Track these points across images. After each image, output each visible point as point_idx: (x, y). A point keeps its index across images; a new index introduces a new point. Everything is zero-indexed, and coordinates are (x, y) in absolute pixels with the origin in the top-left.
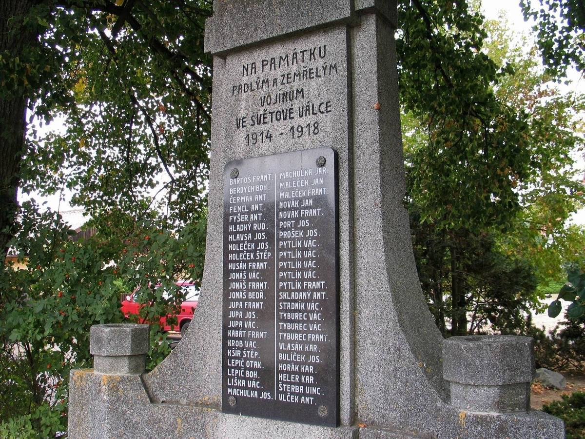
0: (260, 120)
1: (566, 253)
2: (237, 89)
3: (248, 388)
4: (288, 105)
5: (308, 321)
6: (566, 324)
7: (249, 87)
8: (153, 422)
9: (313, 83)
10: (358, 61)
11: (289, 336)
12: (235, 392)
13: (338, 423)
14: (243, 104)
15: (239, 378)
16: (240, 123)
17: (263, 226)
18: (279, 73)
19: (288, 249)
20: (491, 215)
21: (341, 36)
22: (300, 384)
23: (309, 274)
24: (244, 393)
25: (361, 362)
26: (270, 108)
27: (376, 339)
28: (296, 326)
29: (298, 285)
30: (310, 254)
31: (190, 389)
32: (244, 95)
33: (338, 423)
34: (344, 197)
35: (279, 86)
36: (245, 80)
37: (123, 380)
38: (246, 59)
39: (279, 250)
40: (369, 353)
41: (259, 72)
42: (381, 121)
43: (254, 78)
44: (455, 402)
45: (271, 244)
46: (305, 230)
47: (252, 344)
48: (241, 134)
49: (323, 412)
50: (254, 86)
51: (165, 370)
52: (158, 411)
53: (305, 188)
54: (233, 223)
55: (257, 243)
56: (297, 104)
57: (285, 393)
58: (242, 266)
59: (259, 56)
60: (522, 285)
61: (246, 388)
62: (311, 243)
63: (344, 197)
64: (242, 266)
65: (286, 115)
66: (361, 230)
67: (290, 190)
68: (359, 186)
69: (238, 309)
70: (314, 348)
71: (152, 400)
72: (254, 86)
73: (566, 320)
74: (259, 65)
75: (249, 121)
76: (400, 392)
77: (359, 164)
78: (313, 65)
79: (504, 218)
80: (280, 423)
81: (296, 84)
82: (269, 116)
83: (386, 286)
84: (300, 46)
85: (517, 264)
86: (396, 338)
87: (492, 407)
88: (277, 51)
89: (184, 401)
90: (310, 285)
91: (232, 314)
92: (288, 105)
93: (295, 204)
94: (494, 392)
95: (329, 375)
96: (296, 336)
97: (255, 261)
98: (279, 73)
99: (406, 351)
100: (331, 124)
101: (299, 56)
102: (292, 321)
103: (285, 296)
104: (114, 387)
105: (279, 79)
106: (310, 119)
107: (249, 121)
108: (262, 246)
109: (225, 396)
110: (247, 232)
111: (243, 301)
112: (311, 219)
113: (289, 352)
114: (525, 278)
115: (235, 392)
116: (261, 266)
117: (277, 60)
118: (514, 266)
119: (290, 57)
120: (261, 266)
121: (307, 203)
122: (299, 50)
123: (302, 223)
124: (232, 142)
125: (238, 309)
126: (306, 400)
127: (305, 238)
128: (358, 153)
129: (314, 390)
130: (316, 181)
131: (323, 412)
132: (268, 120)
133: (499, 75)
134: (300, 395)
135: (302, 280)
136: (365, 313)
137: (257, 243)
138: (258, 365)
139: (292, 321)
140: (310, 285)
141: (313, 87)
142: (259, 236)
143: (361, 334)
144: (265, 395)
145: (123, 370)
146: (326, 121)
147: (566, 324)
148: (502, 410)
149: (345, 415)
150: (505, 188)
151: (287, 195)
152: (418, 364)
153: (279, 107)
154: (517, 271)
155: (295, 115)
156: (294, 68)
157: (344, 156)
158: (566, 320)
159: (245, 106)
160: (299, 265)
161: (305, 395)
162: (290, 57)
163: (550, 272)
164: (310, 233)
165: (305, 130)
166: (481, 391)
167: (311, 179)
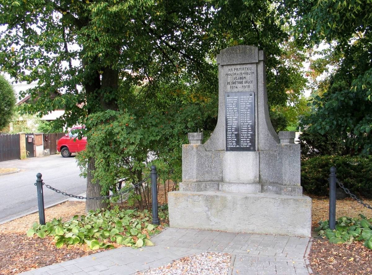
0: (234, 83)
1: (299, 111)
2: (227, 75)
3: (234, 145)
4: (242, 80)
5: (248, 129)
6: (299, 141)
7: (231, 75)
8: (206, 156)
9: (248, 76)
10: (259, 72)
11: (243, 133)
12: (230, 146)
13: (255, 151)
14: (229, 79)
15: (230, 143)
16: (228, 83)
17: (236, 109)
18: (239, 72)
19: (243, 114)
20: (279, 101)
21: (255, 66)
22: (246, 143)
23: (248, 119)
24: (232, 146)
25: (259, 138)
26: (237, 81)
27: (263, 133)
28: (245, 131)
29: (246, 122)
30: (248, 115)
31: (215, 147)
32: (229, 77)
33: (255, 151)
34: (256, 103)
35: (233, 71)
36: (229, 73)
37: (199, 146)
38: (230, 67)
39: (241, 114)
40: (261, 136)
41: (233, 71)
42: (264, 86)
43: (232, 72)
44: (281, 143)
45: (239, 112)
46: (247, 110)
47: (234, 135)
48: (229, 86)
49: (252, 148)
50: (232, 75)
51: (208, 143)
52: (208, 153)
53: (247, 100)
54: (228, 107)
55: (235, 112)
56: (244, 81)
57: (243, 145)
58: (231, 117)
59: (233, 67)
60: (281, 125)
61: (232, 145)
62: (248, 113)
63: (256, 103)
64: (231, 117)
65: (241, 83)
66: (259, 110)
67: (243, 101)
68: (259, 100)
69: (230, 127)
70: (249, 135)
71: (206, 151)
72: (232, 75)
73: (299, 140)
74: (233, 69)
75: (231, 83)
76: (268, 143)
77: (259, 95)
78: (248, 71)
79: (283, 102)
80: (241, 152)
81: (244, 76)
82: (236, 83)
83: (265, 122)
84: (244, 66)
85: (279, 116)
86: (267, 132)
87: (288, 143)
88: (238, 67)
89: (213, 150)
90: (249, 122)
91: (228, 129)
92: (242, 80)
93: (245, 104)
94: (289, 140)
95: (253, 141)
96: (245, 133)
97: (234, 116)
98: (239, 72)
99: (270, 135)
100: (252, 86)
101: (244, 69)
102: (244, 129)
103: (242, 124)
104: (197, 148)
105: (239, 74)
106: (247, 84)
107: (231, 83)
108: (236, 113)
109: (227, 147)
110: (232, 110)
111: (231, 125)
112: (248, 107)
113: (243, 136)
114: (283, 122)
115: (230, 146)
116: (236, 117)
117: (238, 69)
118: (278, 117)
119: (242, 69)
120: (236, 117)
121: (247, 104)
122: (244, 67)
123: (246, 108)
124: (226, 88)
125: (230, 127)
126: (247, 146)
127: (247, 111)
128: (259, 93)
129: (250, 144)
130: (250, 99)
131: (252, 148)
132: (236, 83)
133: (282, 54)
134: (246, 145)
135: (247, 121)
136: (260, 127)
137: (235, 112)
138: (235, 140)
139: (244, 129)
140: (249, 122)
141: (248, 77)
142: (235, 111)
143: (259, 132)
144: (237, 146)
145: (199, 143)
146: (251, 85)
147: (299, 141)
148: (290, 143)
149: (256, 149)
150: (282, 90)
151: (242, 102)
152: (272, 137)
153: (239, 80)
154: (280, 119)
155: (244, 83)
156: (243, 72)
157: (256, 93)
158: (299, 140)
159: (230, 79)
160: (246, 117)
161: (247, 145)
162: (242, 69)
163: (292, 119)
164: (248, 110)
165: (246, 87)
166: (286, 140)
167: (248, 98)
